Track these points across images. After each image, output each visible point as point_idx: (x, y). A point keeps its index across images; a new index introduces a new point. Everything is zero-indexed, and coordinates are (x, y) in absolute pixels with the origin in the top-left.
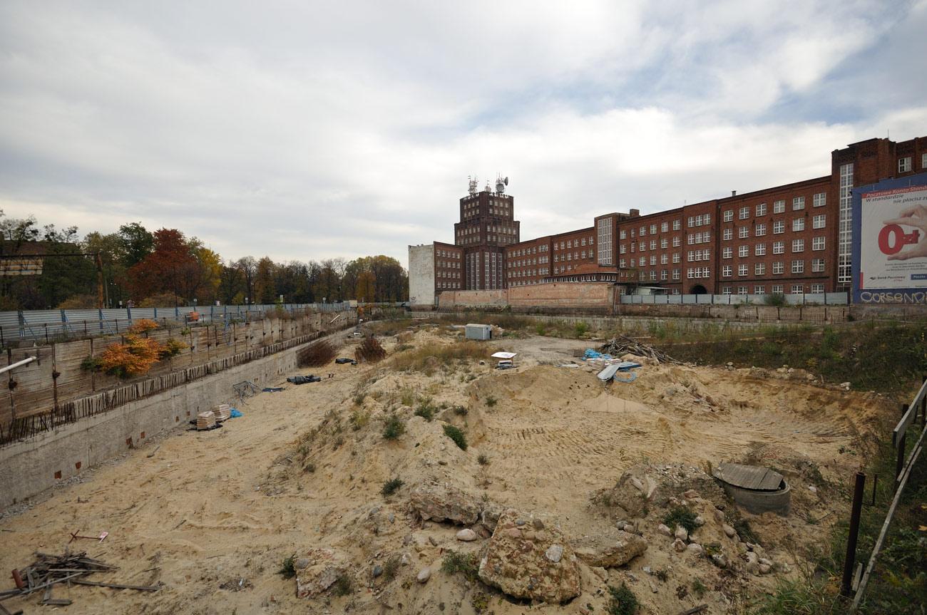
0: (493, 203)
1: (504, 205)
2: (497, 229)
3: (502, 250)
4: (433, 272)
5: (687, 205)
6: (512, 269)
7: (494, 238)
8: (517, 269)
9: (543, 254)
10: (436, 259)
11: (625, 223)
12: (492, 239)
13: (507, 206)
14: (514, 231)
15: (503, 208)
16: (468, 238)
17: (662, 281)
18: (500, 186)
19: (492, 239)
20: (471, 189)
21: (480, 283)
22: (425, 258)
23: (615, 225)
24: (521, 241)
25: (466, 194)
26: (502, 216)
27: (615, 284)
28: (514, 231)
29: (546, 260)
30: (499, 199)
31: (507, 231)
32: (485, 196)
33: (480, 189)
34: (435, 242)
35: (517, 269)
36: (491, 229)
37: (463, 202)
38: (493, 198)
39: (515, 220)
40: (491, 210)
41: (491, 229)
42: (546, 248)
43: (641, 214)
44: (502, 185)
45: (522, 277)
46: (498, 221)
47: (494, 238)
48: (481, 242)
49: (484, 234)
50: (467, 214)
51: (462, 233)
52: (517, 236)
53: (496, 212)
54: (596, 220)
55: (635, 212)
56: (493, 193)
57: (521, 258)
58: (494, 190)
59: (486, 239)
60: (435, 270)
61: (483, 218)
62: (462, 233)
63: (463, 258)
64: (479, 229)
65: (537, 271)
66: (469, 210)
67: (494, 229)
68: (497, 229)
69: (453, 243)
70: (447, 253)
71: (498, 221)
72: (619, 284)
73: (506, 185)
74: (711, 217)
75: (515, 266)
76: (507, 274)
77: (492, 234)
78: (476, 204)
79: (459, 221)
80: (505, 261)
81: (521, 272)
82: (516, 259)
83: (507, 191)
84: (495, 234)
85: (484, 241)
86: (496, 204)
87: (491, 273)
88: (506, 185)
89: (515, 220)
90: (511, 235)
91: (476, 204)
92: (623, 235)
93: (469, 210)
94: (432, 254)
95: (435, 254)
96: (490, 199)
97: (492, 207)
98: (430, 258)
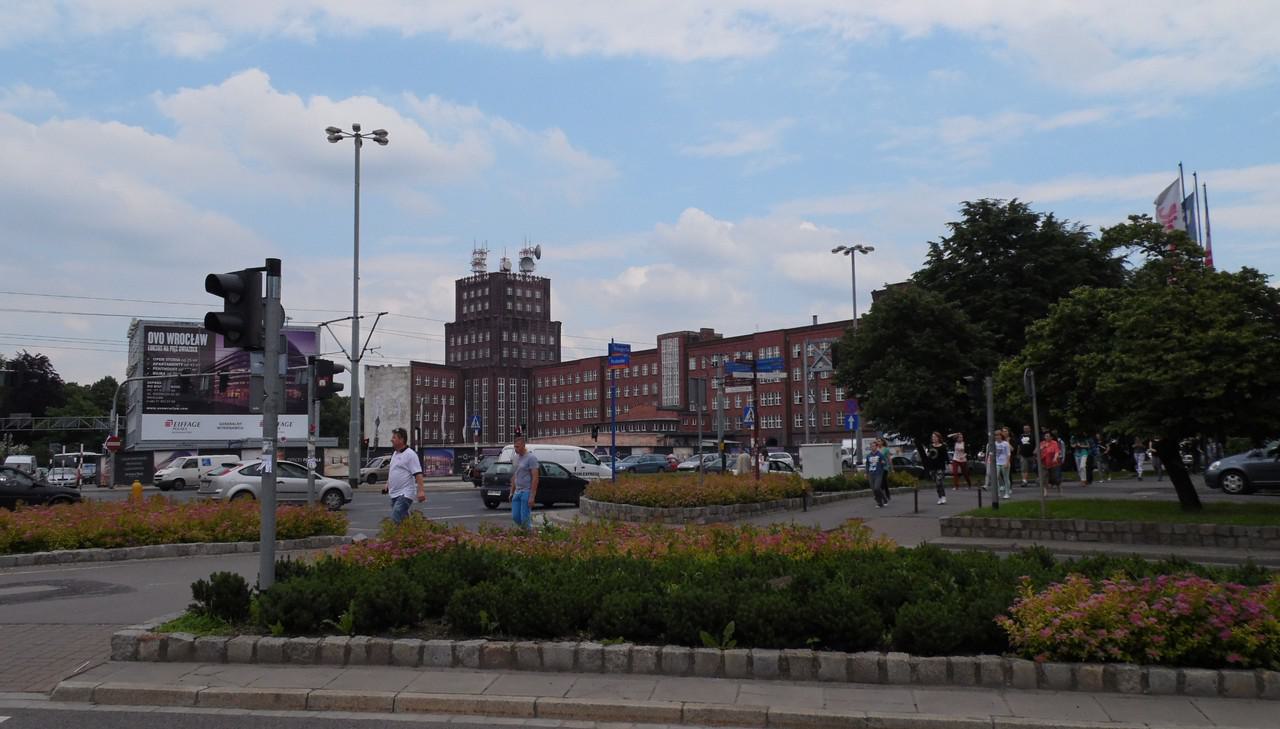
0: (514, 291)
1: (533, 294)
2: (519, 337)
3: (528, 373)
4: (409, 412)
5: (761, 330)
6: (544, 408)
7: (515, 353)
8: (552, 408)
9: (590, 385)
10: (415, 390)
11: (697, 344)
12: (510, 354)
13: (538, 295)
14: (552, 339)
15: (532, 300)
16: (470, 351)
17: (737, 432)
18: (526, 261)
19: (510, 354)
20: (477, 263)
21: (489, 430)
22: (395, 389)
23: (682, 349)
24: (563, 359)
25: (468, 272)
26: (529, 314)
27: (666, 437)
28: (552, 339)
29: (592, 394)
30: (524, 285)
31: (538, 340)
32: (502, 279)
33: (492, 266)
34: (268, 260)
35: (552, 408)
36: (510, 337)
37: (461, 286)
38: (513, 283)
39: (552, 320)
40: (509, 305)
41: (510, 337)
42: (591, 376)
43: (724, 337)
44: (530, 260)
45: (551, 421)
46: (520, 323)
47: (515, 353)
48: (491, 358)
49: (497, 345)
50: (469, 308)
51: (459, 340)
52: (557, 348)
53: (519, 306)
54: (660, 339)
55: (710, 332)
56: (515, 275)
57: (557, 389)
58: (515, 269)
59: (501, 354)
60: (412, 409)
61: (496, 318)
62: (459, 340)
63: (460, 387)
64: (488, 336)
65: (582, 411)
66: (471, 301)
67: (515, 336)
68: (519, 337)
69: (442, 362)
70: (423, 379)
71: (520, 323)
72: (672, 436)
73: (538, 258)
74: (780, 351)
75: (548, 402)
76: (536, 417)
77: (511, 344)
78: (483, 292)
79: (452, 319)
80: (533, 392)
81: (574, 413)
82: (550, 390)
83: (539, 270)
84: (517, 345)
85: (496, 358)
86: (519, 292)
87: (134, 461)
88: (538, 258)
89: (552, 320)
90: (544, 346)
91: (483, 292)
92: (692, 365)
93: (471, 301)
94: (406, 383)
95: (413, 382)
96: (509, 286)
97: (512, 298)
98: (403, 389)
